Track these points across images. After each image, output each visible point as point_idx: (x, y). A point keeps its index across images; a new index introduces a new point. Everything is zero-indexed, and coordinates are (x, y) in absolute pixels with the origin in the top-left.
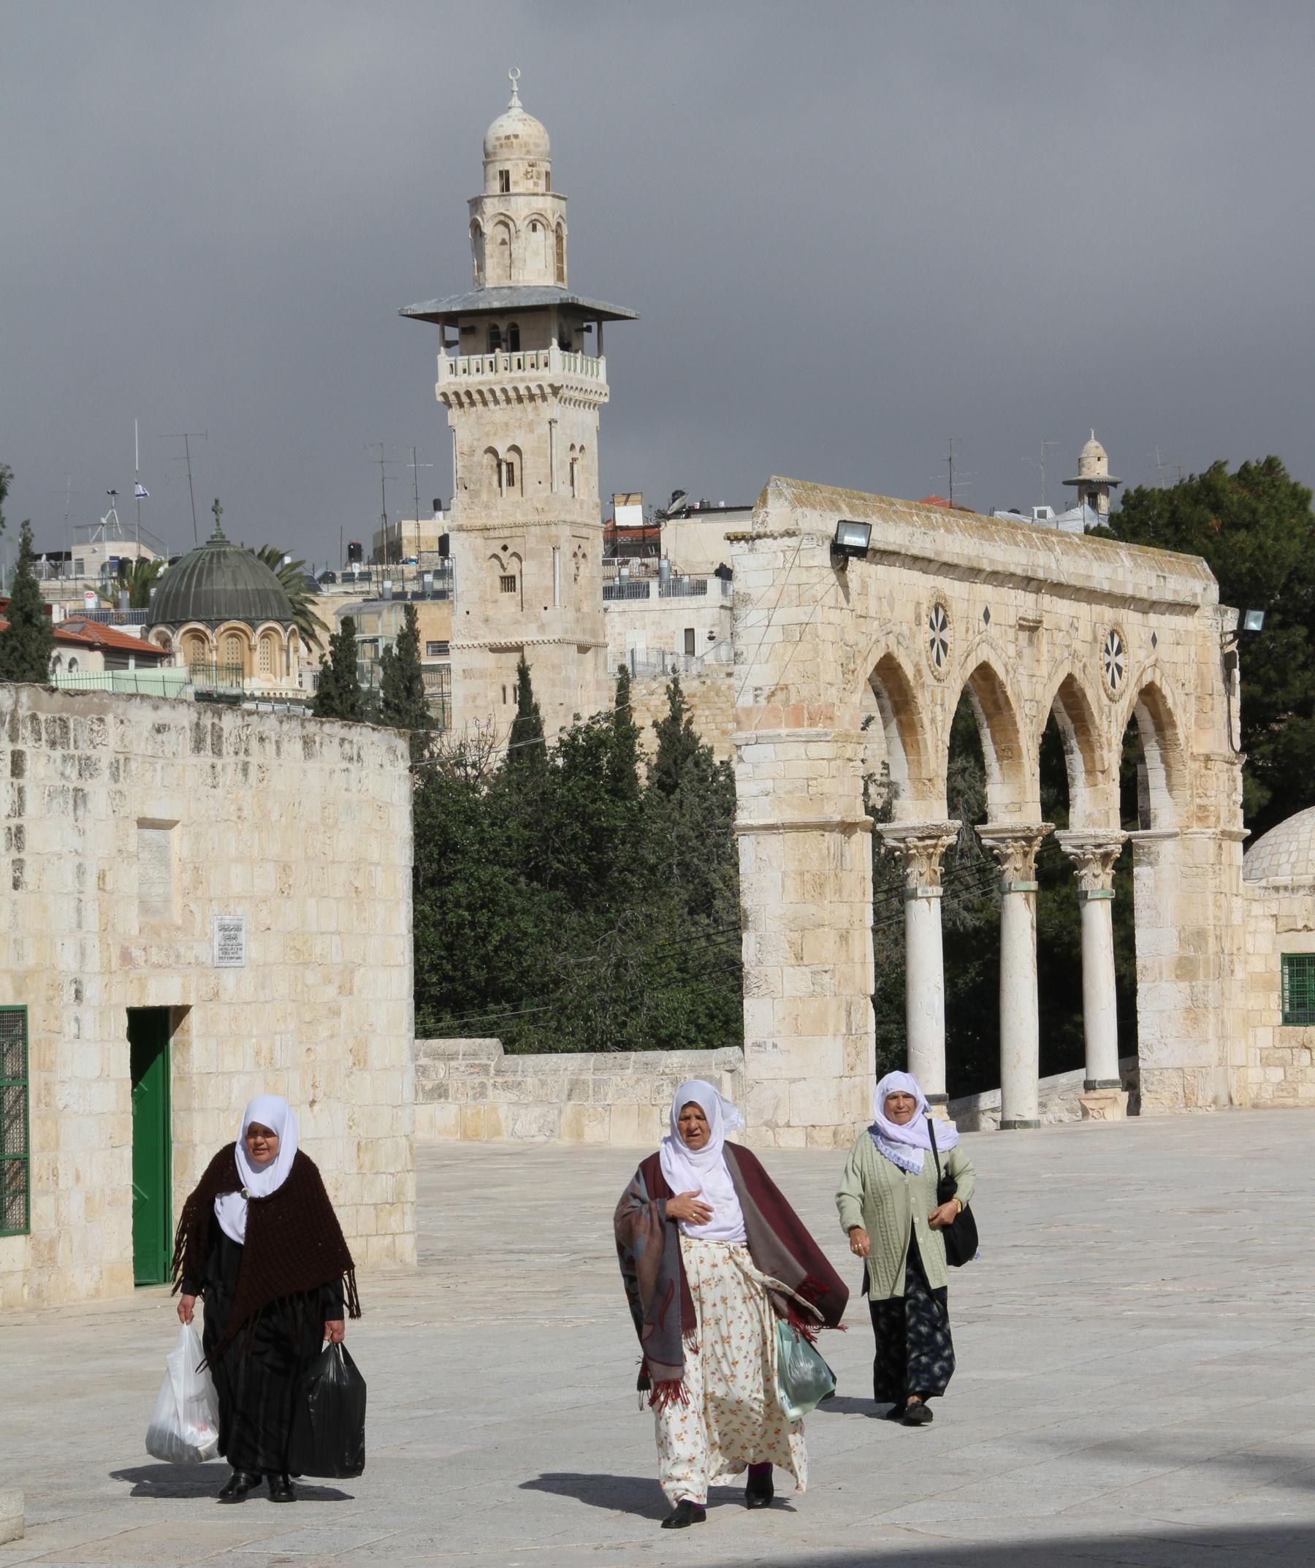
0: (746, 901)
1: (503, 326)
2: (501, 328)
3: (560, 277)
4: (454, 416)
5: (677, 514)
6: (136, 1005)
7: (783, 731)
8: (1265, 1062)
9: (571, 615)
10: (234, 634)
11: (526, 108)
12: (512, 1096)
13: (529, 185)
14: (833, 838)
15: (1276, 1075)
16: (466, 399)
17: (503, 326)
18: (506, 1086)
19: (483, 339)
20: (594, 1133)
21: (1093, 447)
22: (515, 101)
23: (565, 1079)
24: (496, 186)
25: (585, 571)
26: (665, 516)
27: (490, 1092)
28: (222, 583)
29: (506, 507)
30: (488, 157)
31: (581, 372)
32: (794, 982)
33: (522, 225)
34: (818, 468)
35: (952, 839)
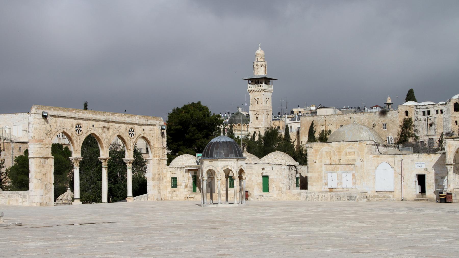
0: (30, 169)
1: (257, 81)
2: (257, 81)
3: (265, 73)
4: (250, 94)
5: (320, 108)
8: (169, 194)
9: (266, 123)
10: (239, 125)
11: (261, 49)
13: (261, 60)
14: (43, 159)
15: (170, 195)
16: (251, 91)
17: (257, 81)
19: (254, 82)
20: (11, 203)
21: (389, 98)
22: (260, 48)
23: (8, 194)
24: (256, 60)
25: (269, 117)
26: (318, 108)
29: (257, 107)
30: (256, 56)
31: (270, 87)
33: (259, 66)
34: (42, 103)
35: (81, 160)
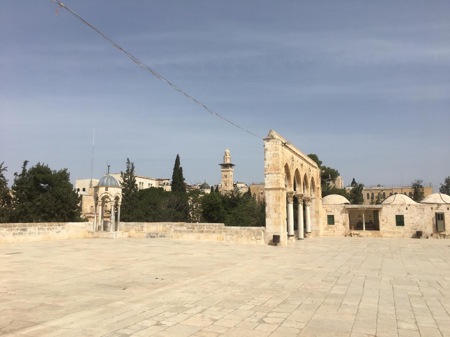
6: (401, 227)
7: (273, 172)
12: (225, 233)
18: (225, 232)
27: (222, 232)
28: (205, 186)
32: (274, 215)
